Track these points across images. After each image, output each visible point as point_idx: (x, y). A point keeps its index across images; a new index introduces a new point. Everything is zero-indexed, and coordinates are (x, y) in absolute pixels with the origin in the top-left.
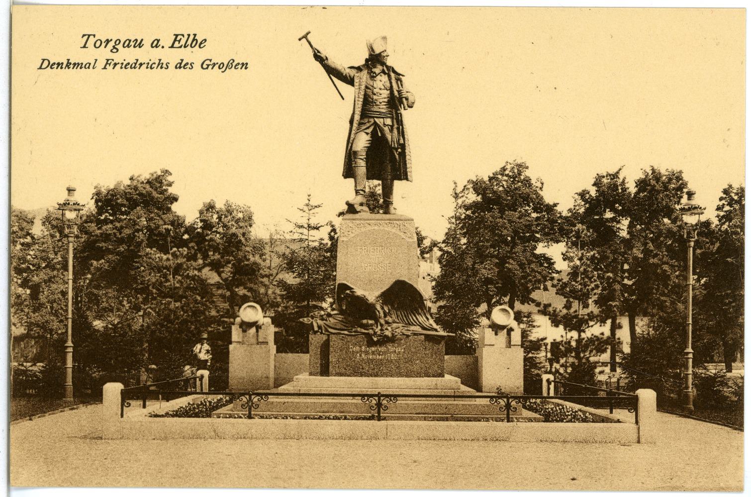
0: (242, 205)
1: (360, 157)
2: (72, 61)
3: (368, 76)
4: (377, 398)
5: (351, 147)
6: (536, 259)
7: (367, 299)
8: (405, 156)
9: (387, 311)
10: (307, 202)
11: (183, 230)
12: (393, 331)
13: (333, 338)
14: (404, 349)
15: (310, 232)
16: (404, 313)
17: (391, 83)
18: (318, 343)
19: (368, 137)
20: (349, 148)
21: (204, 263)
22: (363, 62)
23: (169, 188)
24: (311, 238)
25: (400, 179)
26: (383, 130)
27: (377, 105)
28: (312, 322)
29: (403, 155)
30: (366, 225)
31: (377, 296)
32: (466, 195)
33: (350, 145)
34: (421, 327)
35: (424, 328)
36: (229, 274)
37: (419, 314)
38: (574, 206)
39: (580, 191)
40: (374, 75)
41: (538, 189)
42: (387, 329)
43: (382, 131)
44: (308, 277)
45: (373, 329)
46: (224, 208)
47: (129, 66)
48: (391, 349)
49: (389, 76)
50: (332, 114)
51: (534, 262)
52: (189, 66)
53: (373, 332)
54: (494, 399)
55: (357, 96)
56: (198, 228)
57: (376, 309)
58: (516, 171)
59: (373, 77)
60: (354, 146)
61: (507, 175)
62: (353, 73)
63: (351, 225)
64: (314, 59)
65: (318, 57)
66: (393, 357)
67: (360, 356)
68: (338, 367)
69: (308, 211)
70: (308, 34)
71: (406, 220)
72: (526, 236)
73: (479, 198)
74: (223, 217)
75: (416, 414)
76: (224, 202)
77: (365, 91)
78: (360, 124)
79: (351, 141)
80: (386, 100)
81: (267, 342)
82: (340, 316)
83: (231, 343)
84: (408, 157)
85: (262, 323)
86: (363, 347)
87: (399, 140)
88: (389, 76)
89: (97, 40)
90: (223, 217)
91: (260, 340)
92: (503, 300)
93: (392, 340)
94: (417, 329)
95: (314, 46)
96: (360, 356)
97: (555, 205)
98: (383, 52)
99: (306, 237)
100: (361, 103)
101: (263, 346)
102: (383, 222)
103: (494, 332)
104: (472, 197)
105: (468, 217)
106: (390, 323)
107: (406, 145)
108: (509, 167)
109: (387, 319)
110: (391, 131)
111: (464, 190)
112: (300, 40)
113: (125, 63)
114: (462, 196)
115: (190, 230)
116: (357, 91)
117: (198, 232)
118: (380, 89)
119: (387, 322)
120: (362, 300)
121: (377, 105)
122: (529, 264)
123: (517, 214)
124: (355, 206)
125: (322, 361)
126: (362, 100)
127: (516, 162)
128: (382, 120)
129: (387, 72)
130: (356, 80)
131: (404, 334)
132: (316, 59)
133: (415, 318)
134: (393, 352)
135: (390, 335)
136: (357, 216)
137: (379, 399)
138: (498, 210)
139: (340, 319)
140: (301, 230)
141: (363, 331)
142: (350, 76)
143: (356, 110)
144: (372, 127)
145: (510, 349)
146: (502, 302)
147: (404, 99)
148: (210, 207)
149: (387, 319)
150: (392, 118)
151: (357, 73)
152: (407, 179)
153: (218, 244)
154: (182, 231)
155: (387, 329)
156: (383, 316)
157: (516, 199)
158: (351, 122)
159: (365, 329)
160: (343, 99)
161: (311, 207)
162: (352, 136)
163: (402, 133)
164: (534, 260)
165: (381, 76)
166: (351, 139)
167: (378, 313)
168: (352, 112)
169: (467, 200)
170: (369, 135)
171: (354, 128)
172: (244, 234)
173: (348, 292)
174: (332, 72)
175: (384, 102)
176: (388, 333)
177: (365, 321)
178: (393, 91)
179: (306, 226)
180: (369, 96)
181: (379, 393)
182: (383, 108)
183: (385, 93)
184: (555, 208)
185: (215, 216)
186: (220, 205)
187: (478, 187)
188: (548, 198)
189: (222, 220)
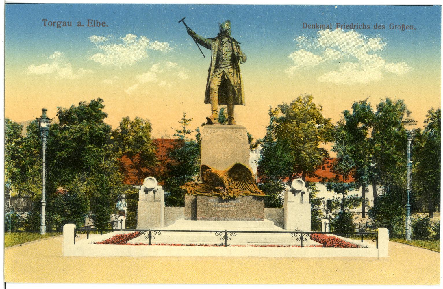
4: (224, 233)
5: (210, 85)
9: (231, 182)
11: (110, 134)
17: (233, 48)
20: (208, 86)
23: (102, 109)
33: (208, 86)
36: (138, 160)
41: (319, 110)
42: (230, 192)
45: (222, 192)
49: (232, 45)
51: (317, 153)
55: (213, 55)
56: (119, 133)
58: (306, 99)
67: (215, 208)
74: (134, 126)
78: (215, 72)
79: (209, 82)
80: (230, 58)
82: (203, 185)
85: (157, 189)
88: (232, 45)
90: (134, 126)
96: (215, 208)
104: (280, 115)
106: (232, 189)
111: (276, 110)
112: (179, 22)
114: (275, 114)
116: (213, 52)
117: (119, 135)
118: (227, 51)
119: (230, 188)
122: (314, 154)
127: (306, 94)
128: (227, 69)
129: (230, 41)
133: (246, 186)
147: (240, 57)
148: (126, 120)
160: (205, 57)
161: (186, 121)
162: (210, 80)
164: (317, 152)
165: (227, 43)
177: (217, 188)
183: (230, 54)
185: (129, 126)
186: (132, 119)
188: (325, 116)
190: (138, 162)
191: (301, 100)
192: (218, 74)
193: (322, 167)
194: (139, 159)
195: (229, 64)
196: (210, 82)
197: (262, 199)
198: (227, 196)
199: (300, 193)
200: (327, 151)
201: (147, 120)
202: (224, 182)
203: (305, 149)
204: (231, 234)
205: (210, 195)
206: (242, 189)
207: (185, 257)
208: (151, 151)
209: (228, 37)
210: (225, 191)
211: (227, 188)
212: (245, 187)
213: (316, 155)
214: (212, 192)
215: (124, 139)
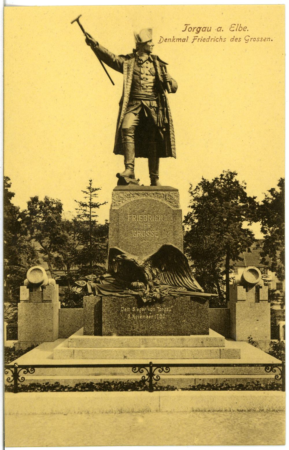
0: (55, 199)
1: (129, 134)
2: (176, 38)
3: (136, 63)
4: (148, 368)
5: (121, 126)
6: (243, 232)
7: (137, 263)
8: (169, 134)
9: (155, 274)
10: (89, 186)
11: (17, 215)
12: (161, 292)
13: (105, 299)
14: (172, 309)
15: (92, 209)
16: (171, 275)
17: (156, 70)
19: (135, 118)
20: (119, 126)
21: (31, 236)
22: (131, 52)
23: (8, 188)
24: (92, 214)
25: (165, 156)
26: (150, 111)
27: (144, 89)
28: (86, 285)
29: (168, 134)
30: (135, 195)
31: (146, 260)
32: (197, 192)
33: (120, 124)
34: (186, 287)
35: (189, 289)
36: (48, 243)
37: (185, 276)
38: (265, 199)
39: (270, 189)
40: (141, 62)
41: (243, 188)
42: (155, 291)
43: (149, 112)
44: (91, 244)
45: (142, 291)
46: (44, 201)
47: (205, 41)
49: (155, 66)
50: (104, 98)
51: (242, 234)
52: (238, 40)
53: (142, 294)
54: (270, 367)
55: (126, 80)
56: (27, 214)
57: (145, 272)
58: (229, 176)
59: (140, 65)
60: (124, 124)
61: (224, 179)
62: (122, 60)
63: (121, 195)
64: (86, 44)
65: (89, 42)
66: (162, 317)
67: (131, 316)
68: (111, 327)
69: (90, 193)
71: (170, 191)
72: (235, 216)
73: (206, 194)
74: (43, 206)
75: (186, 375)
76: (44, 197)
77: (133, 77)
78: (129, 106)
79: (121, 121)
80: (152, 85)
81: (51, 300)
82: (112, 279)
83: (19, 301)
84: (172, 136)
85: (47, 284)
86: (134, 308)
87: (164, 120)
88: (155, 66)
90: (43, 206)
91: (45, 299)
92: (221, 258)
93: (160, 301)
94: (183, 289)
95: (86, 30)
96: (131, 316)
97: (255, 198)
98: (149, 41)
99: (89, 213)
100: (130, 87)
101: (48, 304)
102: (150, 192)
103: (245, 289)
104: (200, 193)
105: (199, 206)
106: (158, 285)
107: (170, 125)
108: (225, 174)
109: (155, 281)
110: (157, 112)
111: (196, 189)
112: (72, 23)
113: (203, 38)
114: (196, 193)
115: (22, 215)
116: (126, 76)
117: (27, 217)
118: (147, 75)
119: (155, 284)
120: (133, 263)
121: (144, 89)
122: (239, 235)
123: (230, 204)
124: (125, 178)
125: (95, 322)
126: (130, 84)
127: (229, 171)
128: (148, 102)
129: (152, 60)
130: (125, 67)
131: (171, 295)
132: (88, 44)
133: (180, 280)
134: (162, 313)
136: (127, 187)
137: (151, 370)
138: (218, 201)
139: (112, 282)
140: (84, 208)
141: (134, 293)
142: (119, 63)
143: (125, 93)
144: (139, 110)
145: (258, 304)
146: (221, 259)
147: (168, 84)
148: (35, 200)
149: (155, 281)
150: (157, 101)
151: (126, 60)
152: (171, 156)
153: (40, 224)
154: (17, 216)
155: (155, 291)
156: (152, 278)
157: (230, 194)
158: (121, 103)
159: (135, 291)
160: (114, 84)
161: (92, 190)
162: (122, 116)
163: (167, 114)
164: (242, 233)
165: (147, 63)
166: (121, 119)
167: (147, 276)
168: (121, 95)
169: (198, 196)
170: (137, 116)
171: (124, 109)
172: (56, 218)
173: (119, 256)
174: (104, 57)
175: (150, 86)
176: (157, 295)
177: (134, 284)
178: (158, 76)
179: (88, 204)
180: (137, 81)
181: (151, 363)
182: (149, 91)
183: (151, 79)
184: (255, 200)
185: (38, 206)
186: (41, 199)
187: (205, 185)
188: (250, 194)
189: (42, 209)
190: (48, 246)
191: (224, 177)
193: (247, 249)
194: (49, 243)
195: (150, 94)
196: (123, 120)
197: (206, 301)
198: (150, 297)
199: (254, 288)
200: (252, 232)
201: (57, 200)
203: (229, 230)
204: (159, 369)
205: (124, 295)
206: (173, 285)
208: (61, 233)
209: (148, 53)
210: (146, 289)
211: (151, 283)
212: (178, 282)
213: (241, 236)
214: (126, 290)
215: (33, 220)
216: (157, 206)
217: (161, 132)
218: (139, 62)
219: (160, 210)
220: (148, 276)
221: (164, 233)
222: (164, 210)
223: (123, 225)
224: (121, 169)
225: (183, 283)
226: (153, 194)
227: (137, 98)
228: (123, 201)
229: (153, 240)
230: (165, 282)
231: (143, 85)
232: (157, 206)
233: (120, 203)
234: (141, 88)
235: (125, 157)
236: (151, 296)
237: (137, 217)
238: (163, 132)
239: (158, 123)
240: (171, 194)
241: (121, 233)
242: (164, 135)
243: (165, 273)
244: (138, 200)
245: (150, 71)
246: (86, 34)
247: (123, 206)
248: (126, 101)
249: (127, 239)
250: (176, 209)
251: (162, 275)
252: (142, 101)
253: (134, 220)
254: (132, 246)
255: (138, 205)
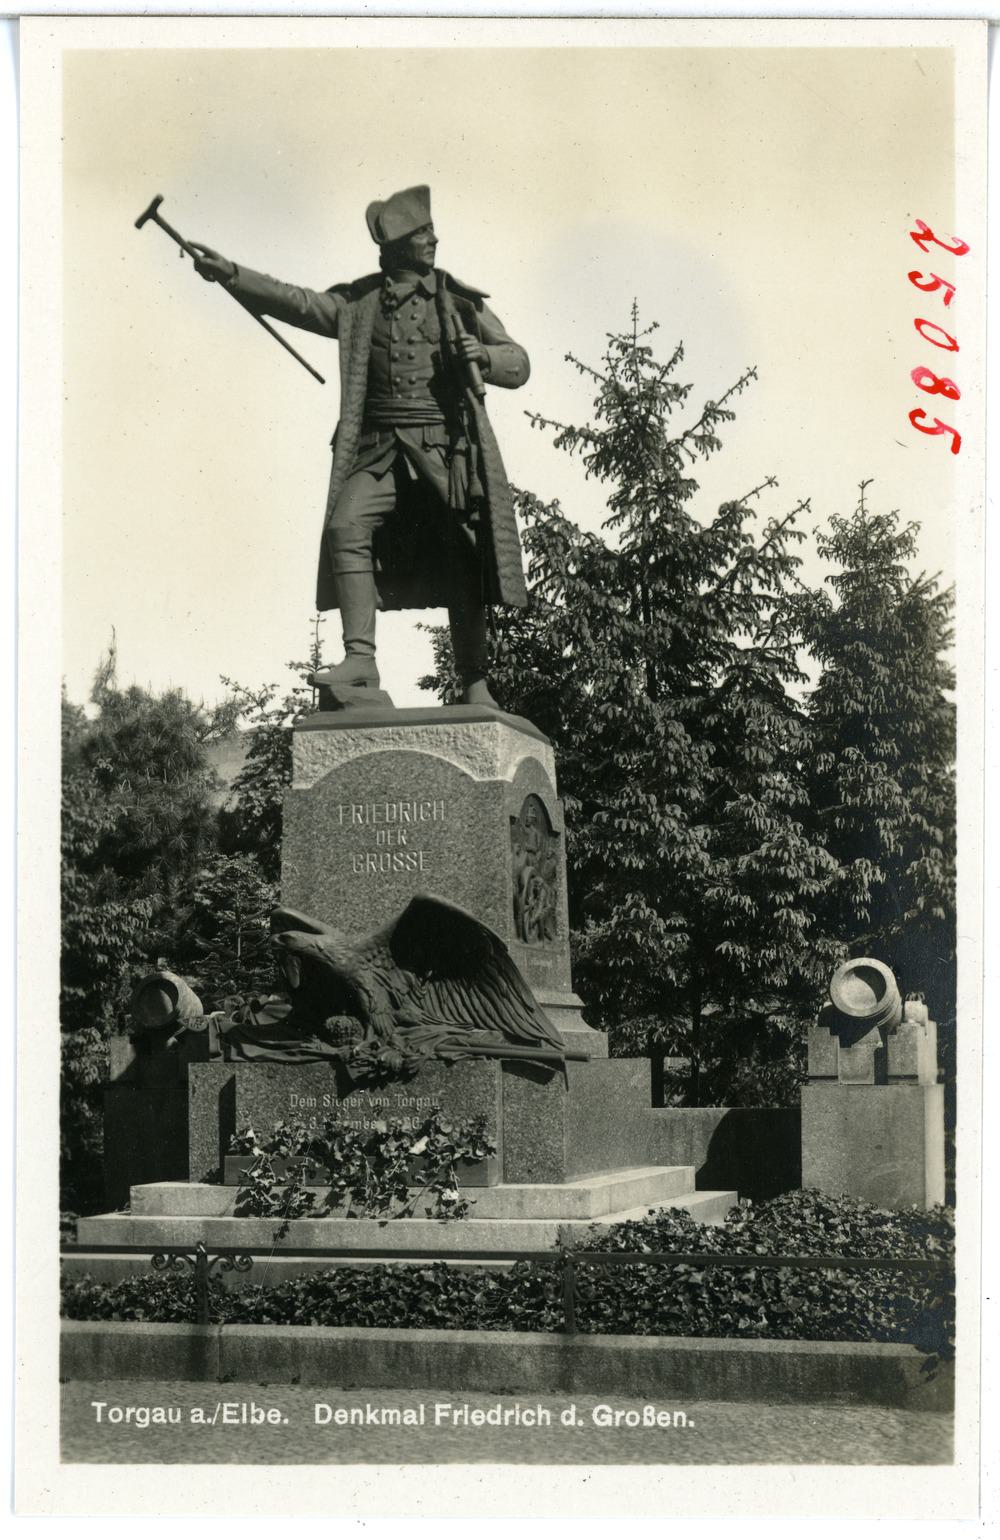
1: (349, 546)
18: (211, 1087)
30: (362, 742)
40: (394, 303)
48: (405, 1102)
49: (440, 310)
63: (320, 743)
65: (210, 268)
70: (157, 201)
88: (440, 310)
89: (915, 424)
95: (186, 238)
102: (408, 729)
112: (139, 224)
130: (345, 324)
132: (207, 277)
135: (398, 1061)
141: (327, 1049)
147: (474, 367)
159: (334, 1046)
160: (322, 381)
192: (372, 458)
198: (370, 1064)
202: (361, 991)
207: (372, 1387)
212: (483, 1014)
216: (427, 772)
217: (465, 526)
218: (387, 302)
219: (435, 785)
220: (370, 996)
221: (449, 859)
222: (448, 785)
223: (323, 838)
224: (334, 653)
225: (514, 1024)
226: (417, 734)
227: (387, 421)
228: (327, 763)
229: (414, 883)
230: (439, 1014)
231: (398, 380)
232: (427, 772)
233: (316, 767)
234: (394, 388)
235: (343, 616)
236: (371, 1059)
237: (364, 809)
238: (472, 525)
239: (453, 496)
240: (472, 732)
241: (317, 864)
242: (476, 534)
243: (441, 986)
244: (368, 757)
245: (423, 328)
246: (188, 248)
247: (324, 779)
248: (349, 436)
249: (338, 882)
250: (487, 779)
251: (429, 991)
252: (398, 431)
253: (357, 819)
254: (351, 903)
255: (367, 772)
